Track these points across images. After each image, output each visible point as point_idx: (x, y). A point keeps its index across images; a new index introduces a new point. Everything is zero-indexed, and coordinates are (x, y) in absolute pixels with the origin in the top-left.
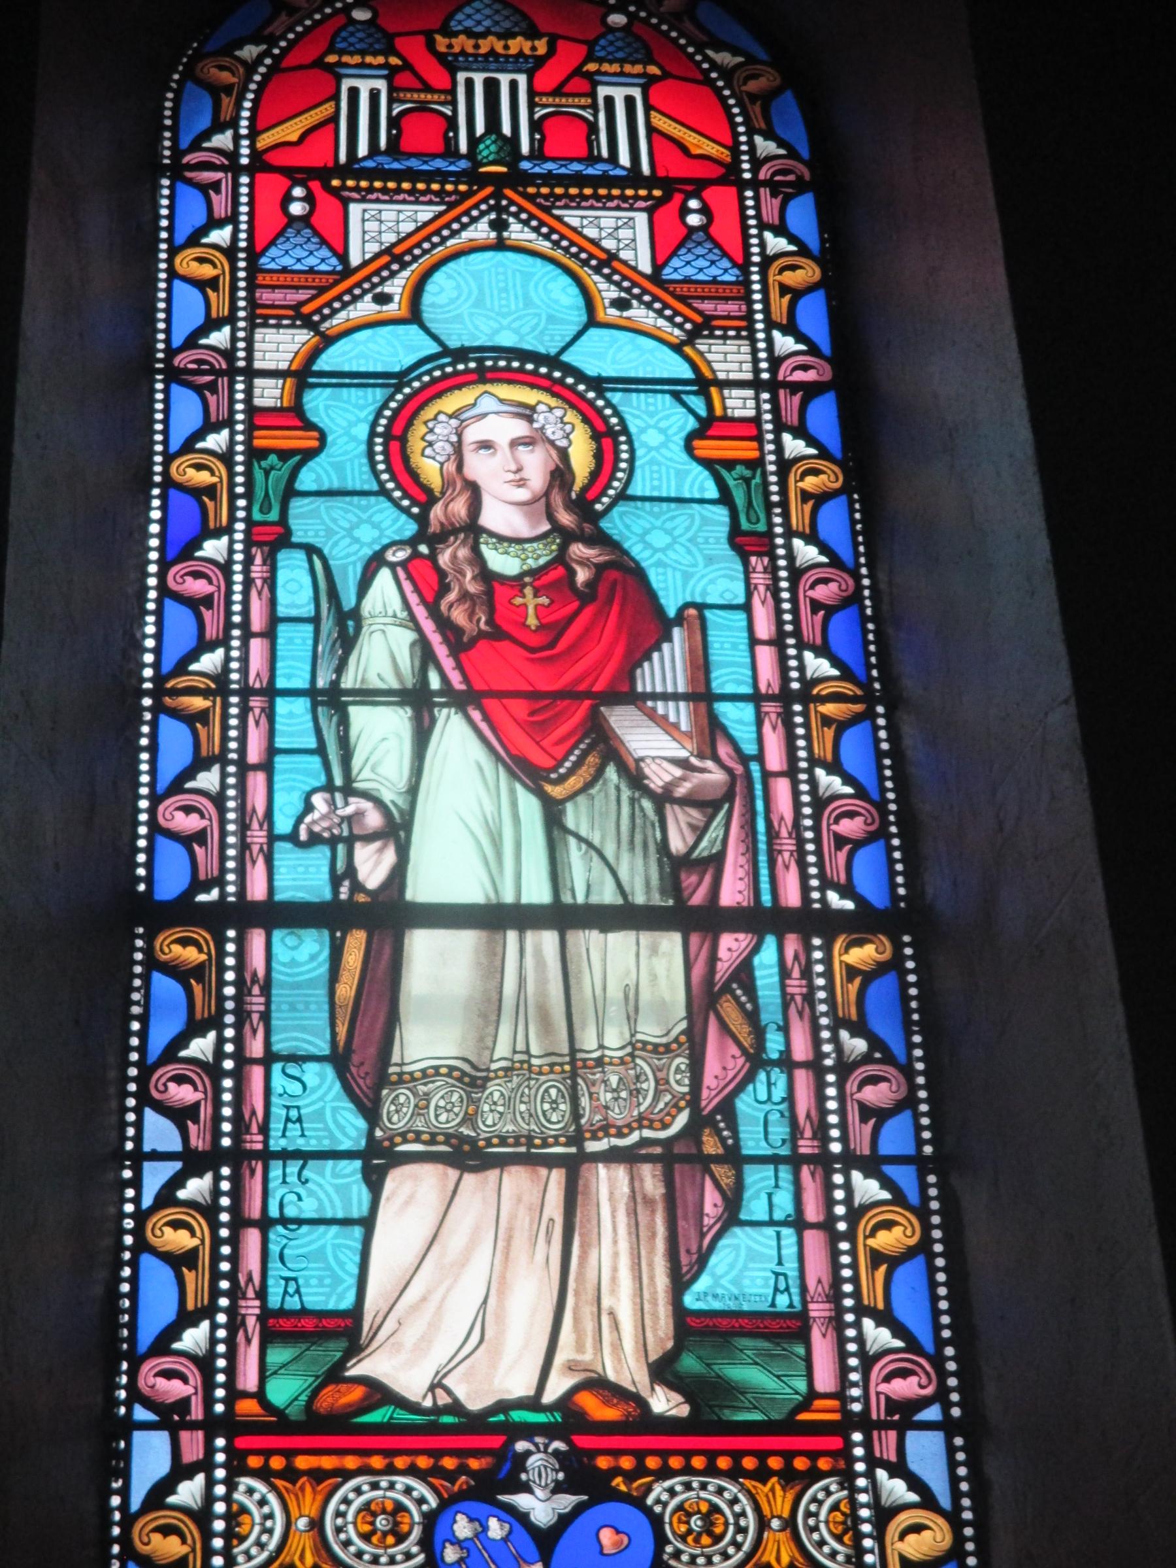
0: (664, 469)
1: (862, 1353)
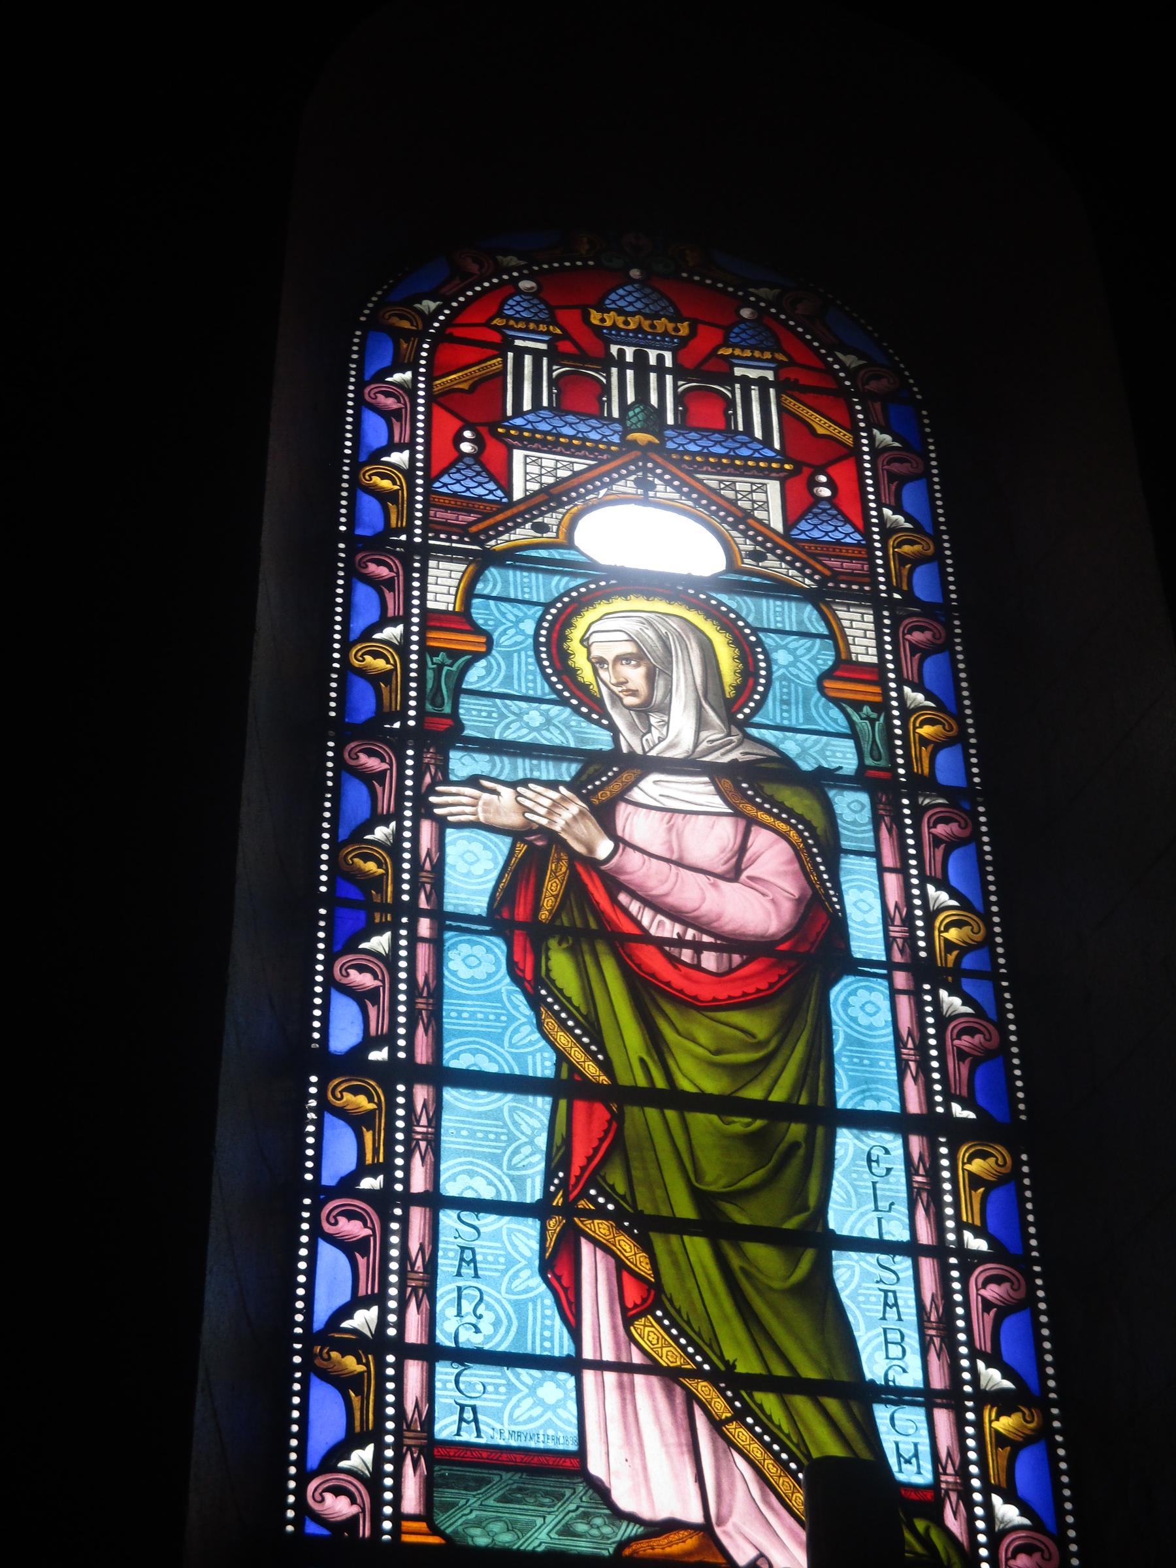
0: (793, 685)
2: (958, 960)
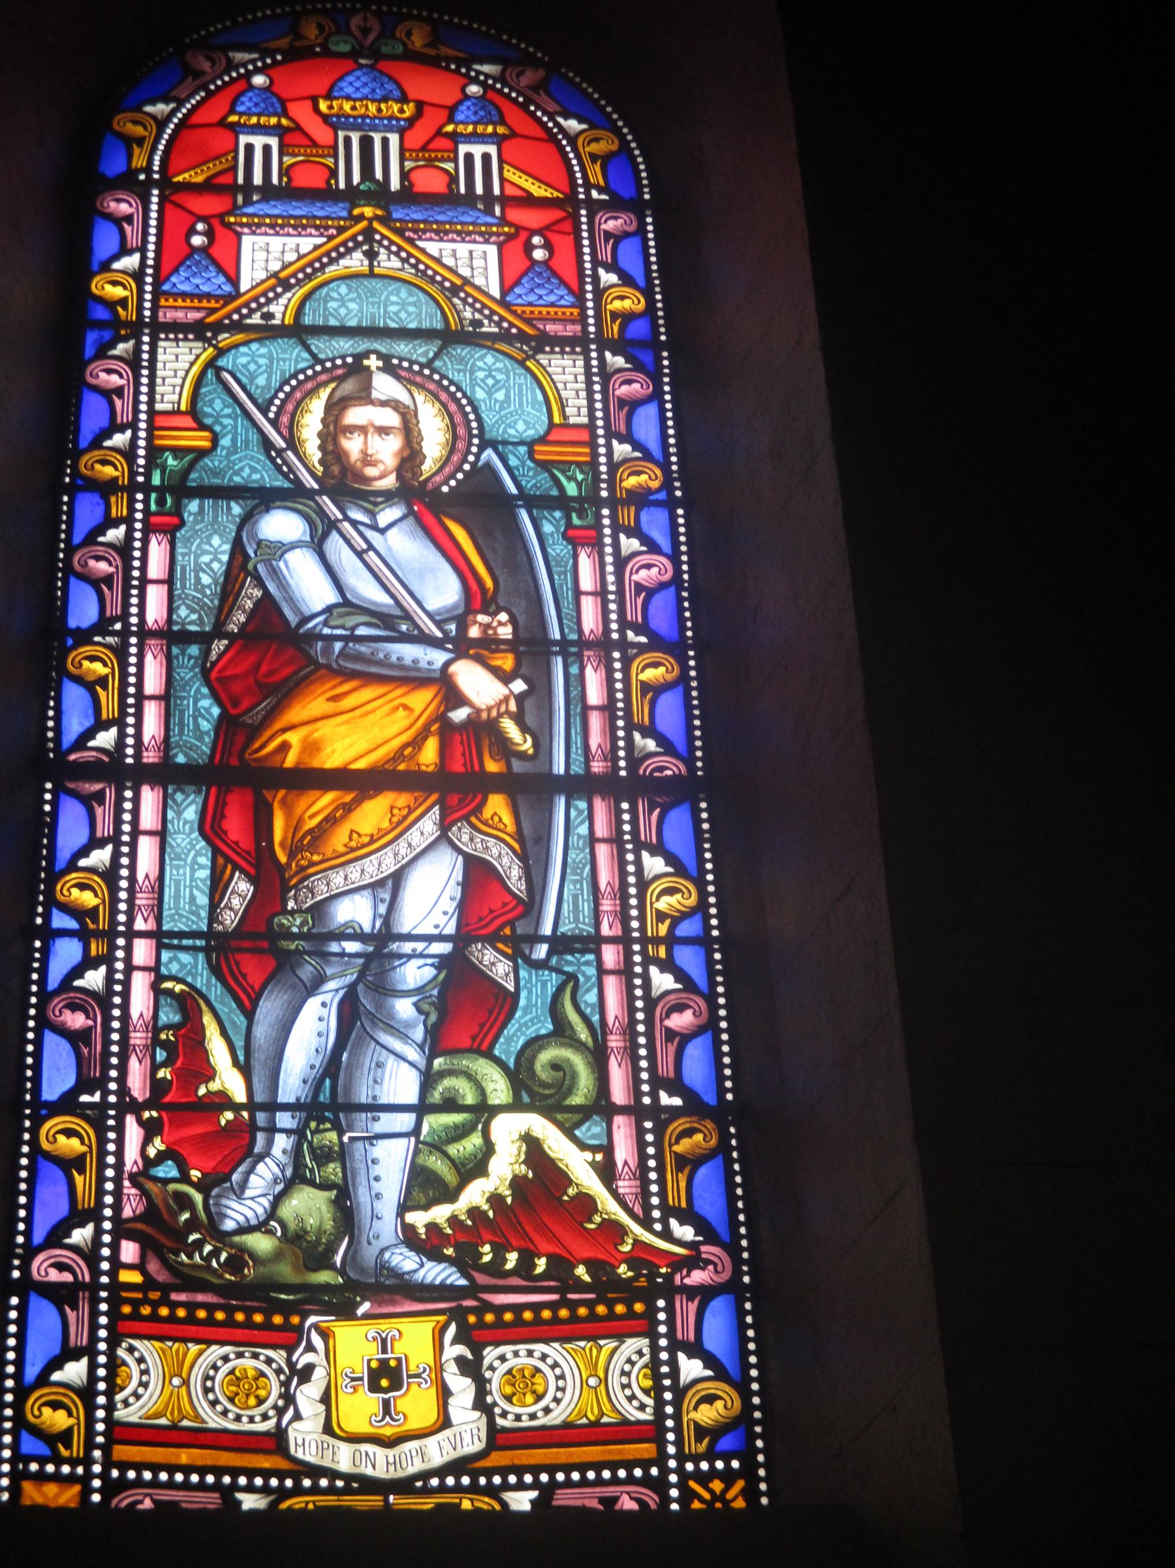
1: (647, 997)
2: (672, 928)
